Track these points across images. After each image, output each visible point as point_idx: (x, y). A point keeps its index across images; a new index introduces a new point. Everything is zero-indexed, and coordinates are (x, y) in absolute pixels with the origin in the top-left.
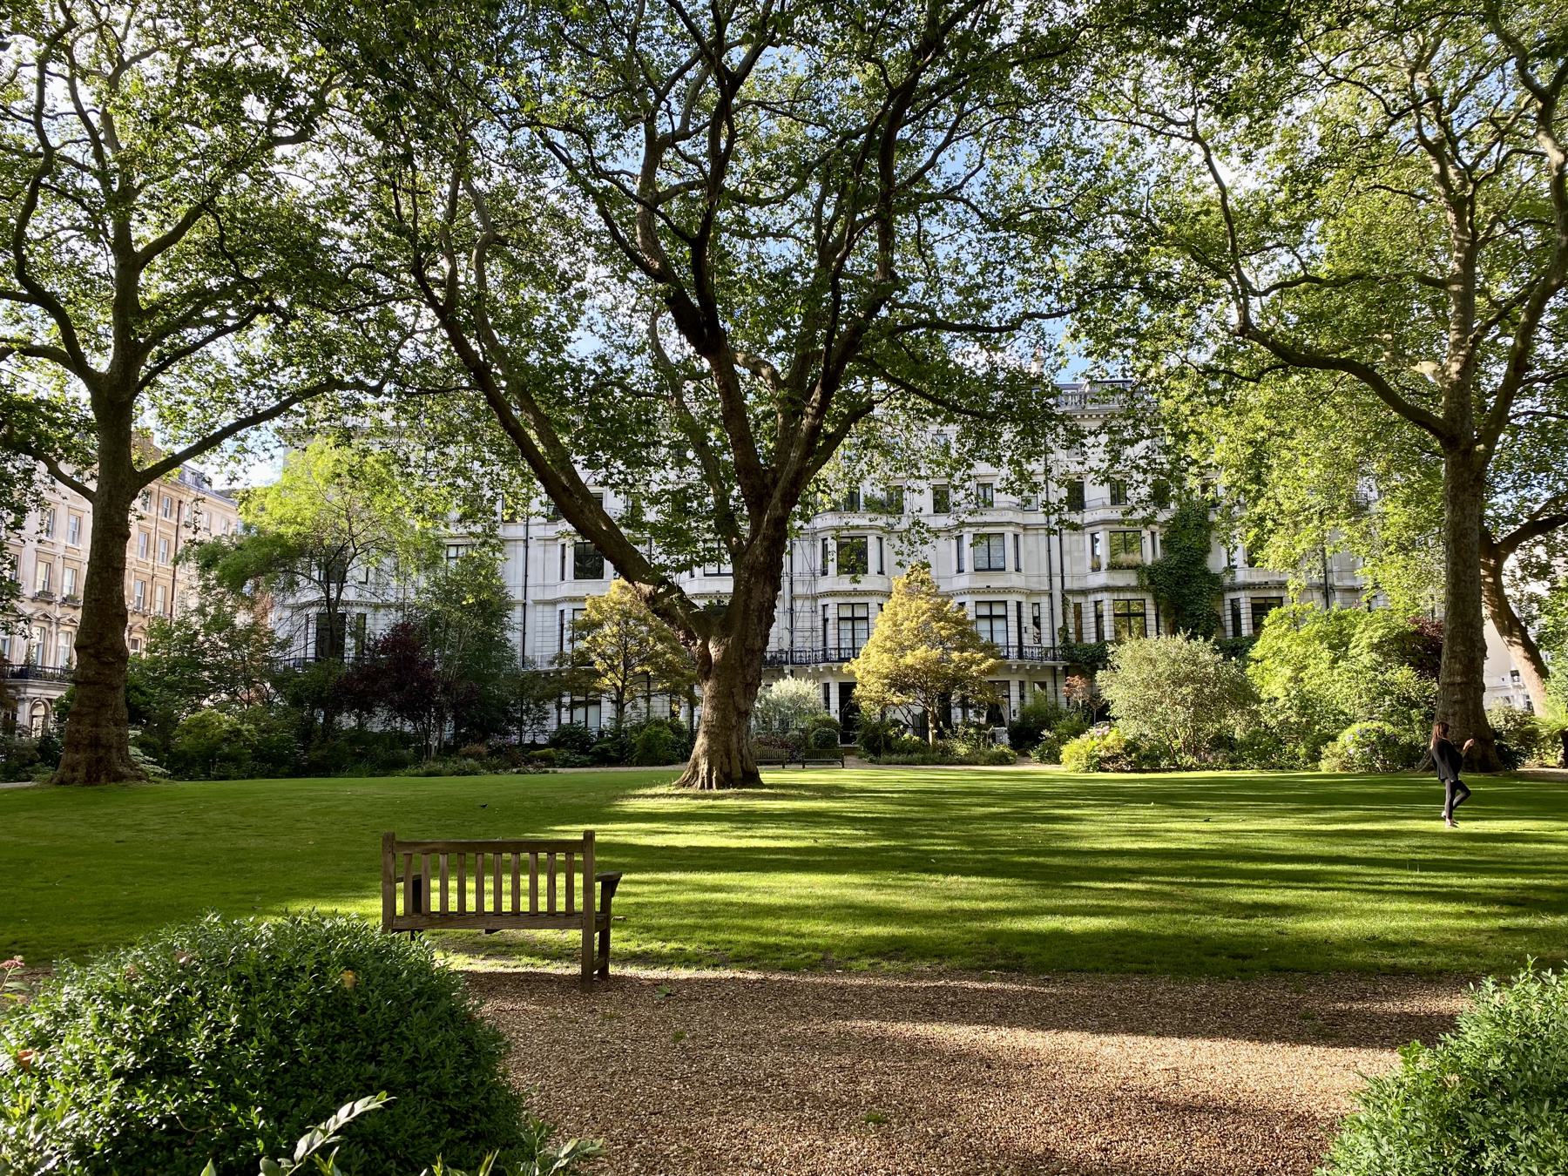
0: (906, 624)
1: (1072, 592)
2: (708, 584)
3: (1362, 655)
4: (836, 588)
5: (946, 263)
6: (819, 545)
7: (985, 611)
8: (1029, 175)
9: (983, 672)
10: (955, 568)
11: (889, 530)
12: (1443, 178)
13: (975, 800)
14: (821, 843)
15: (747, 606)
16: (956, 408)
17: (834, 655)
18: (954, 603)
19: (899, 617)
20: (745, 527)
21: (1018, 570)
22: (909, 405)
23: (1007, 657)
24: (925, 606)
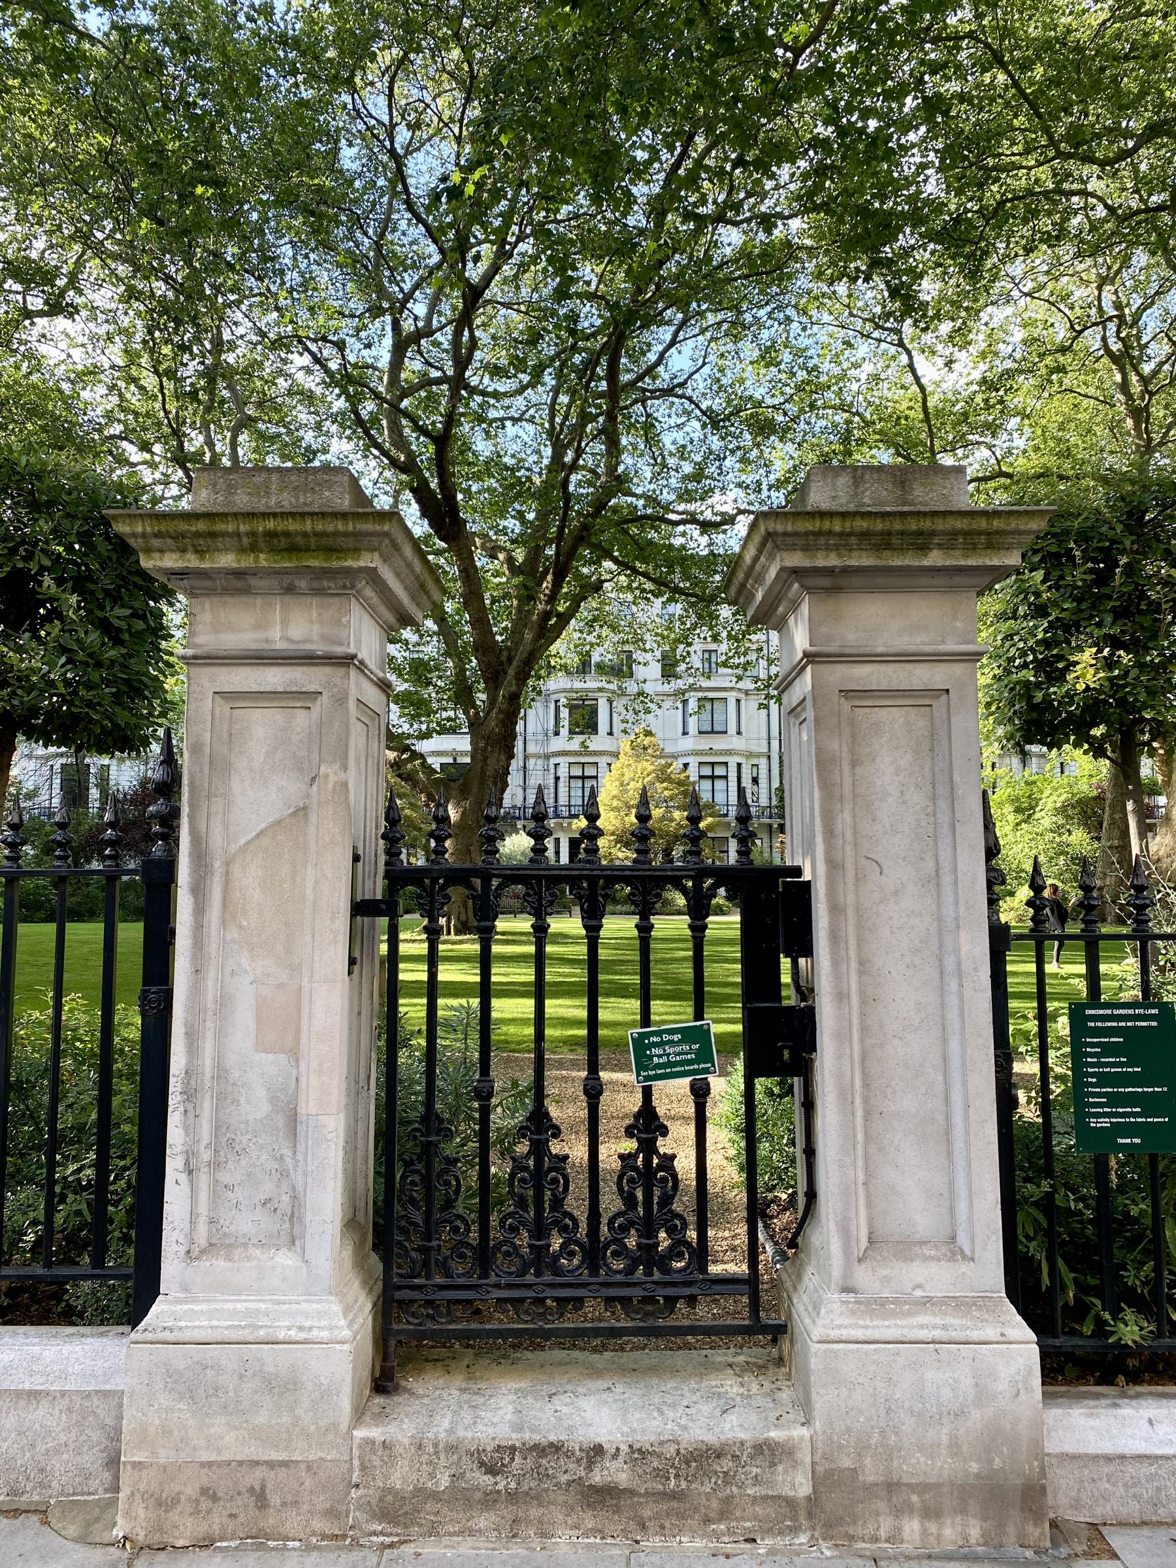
0: (632, 785)
2: (448, 748)
3: (1045, 819)
5: (673, 448)
6: (552, 706)
7: (707, 771)
8: (750, 368)
10: (680, 730)
12: (1124, 387)
13: (680, 945)
15: (483, 773)
16: (677, 590)
17: (564, 811)
18: (677, 765)
19: (626, 778)
20: (481, 697)
21: (739, 733)
23: (726, 815)
24: (651, 768)
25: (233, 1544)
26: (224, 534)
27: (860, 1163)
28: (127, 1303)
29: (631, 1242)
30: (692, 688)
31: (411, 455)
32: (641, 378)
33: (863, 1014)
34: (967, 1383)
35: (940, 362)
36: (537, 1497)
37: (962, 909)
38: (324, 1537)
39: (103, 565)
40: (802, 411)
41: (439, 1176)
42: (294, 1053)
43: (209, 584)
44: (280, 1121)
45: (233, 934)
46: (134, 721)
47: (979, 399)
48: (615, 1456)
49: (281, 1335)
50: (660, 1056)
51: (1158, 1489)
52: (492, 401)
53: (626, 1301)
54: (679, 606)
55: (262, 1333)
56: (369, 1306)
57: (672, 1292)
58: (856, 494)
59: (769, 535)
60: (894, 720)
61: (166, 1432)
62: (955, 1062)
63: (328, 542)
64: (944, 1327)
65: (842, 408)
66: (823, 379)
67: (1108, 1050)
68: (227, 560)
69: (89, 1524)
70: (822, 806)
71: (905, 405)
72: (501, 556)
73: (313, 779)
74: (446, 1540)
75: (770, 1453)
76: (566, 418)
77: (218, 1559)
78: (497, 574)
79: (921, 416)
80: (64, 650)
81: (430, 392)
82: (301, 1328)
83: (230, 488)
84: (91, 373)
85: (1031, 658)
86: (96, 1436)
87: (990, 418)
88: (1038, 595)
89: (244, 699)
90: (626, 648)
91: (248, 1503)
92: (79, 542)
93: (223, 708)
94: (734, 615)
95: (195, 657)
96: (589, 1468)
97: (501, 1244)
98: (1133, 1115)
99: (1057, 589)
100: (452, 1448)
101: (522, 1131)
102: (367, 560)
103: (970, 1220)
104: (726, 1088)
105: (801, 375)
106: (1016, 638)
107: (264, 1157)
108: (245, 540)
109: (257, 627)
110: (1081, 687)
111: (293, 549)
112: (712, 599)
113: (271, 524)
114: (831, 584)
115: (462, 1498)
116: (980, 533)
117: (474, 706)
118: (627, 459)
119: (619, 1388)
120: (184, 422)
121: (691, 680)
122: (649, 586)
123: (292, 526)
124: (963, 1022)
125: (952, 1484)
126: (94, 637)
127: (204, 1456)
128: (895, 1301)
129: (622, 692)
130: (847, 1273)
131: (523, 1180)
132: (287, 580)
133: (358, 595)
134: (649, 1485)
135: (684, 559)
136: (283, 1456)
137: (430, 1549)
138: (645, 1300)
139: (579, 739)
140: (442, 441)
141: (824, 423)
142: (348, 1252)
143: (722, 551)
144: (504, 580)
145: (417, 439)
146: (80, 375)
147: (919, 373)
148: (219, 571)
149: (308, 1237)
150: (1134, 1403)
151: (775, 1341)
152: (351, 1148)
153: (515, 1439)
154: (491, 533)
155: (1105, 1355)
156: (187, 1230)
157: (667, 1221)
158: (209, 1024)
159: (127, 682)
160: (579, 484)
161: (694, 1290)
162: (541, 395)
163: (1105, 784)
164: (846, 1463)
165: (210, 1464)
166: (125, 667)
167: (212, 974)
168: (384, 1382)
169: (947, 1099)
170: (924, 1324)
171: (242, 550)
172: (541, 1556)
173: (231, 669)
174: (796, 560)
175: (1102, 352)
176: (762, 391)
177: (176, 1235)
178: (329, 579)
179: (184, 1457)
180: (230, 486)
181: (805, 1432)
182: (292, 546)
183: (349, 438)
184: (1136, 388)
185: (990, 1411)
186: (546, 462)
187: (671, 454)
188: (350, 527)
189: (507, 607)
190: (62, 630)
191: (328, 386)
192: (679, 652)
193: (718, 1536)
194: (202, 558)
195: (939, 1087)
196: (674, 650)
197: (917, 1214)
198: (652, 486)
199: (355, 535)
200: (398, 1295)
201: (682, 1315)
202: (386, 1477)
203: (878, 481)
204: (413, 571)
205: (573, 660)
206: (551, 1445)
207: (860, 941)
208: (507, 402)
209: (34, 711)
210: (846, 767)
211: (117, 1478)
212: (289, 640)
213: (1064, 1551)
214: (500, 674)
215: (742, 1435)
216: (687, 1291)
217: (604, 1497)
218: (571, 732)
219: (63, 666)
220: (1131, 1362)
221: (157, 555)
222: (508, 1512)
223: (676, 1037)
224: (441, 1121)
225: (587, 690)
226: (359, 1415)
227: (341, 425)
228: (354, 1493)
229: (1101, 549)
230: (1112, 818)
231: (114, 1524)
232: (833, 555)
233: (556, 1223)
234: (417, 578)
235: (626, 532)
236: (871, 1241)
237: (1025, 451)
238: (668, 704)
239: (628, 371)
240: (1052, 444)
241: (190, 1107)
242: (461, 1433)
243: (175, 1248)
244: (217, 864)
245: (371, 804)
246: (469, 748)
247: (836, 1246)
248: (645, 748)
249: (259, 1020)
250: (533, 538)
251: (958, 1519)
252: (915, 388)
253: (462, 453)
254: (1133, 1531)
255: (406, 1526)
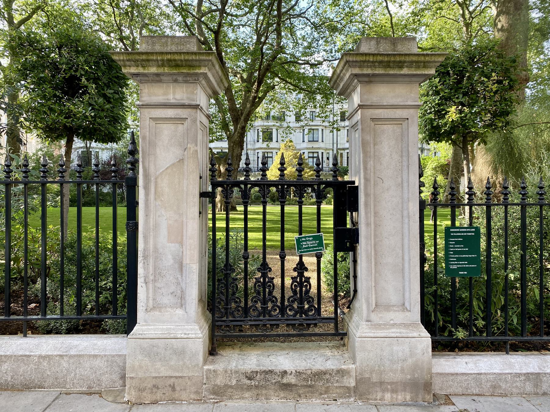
1: (340, 149)
4: (262, 147)
5: (300, 37)
6: (256, 131)
7: (311, 155)
8: (329, 7)
9: (309, 176)
11: (281, 127)
14: (255, 226)
20: (232, 128)
21: (323, 141)
22: (286, 87)
24: (291, 154)
25: (164, 402)
26: (152, 60)
27: (373, 280)
28: (125, 328)
29: (295, 306)
30: (306, 125)
31: (205, 38)
32: (289, 10)
33: (375, 231)
34: (407, 350)
35: (397, 5)
36: (265, 387)
37: (410, 195)
38: (194, 400)
39: (103, 74)
40: (347, 23)
41: (230, 284)
42: (181, 243)
43: (147, 78)
44: (177, 266)
45: (159, 203)
46: (116, 131)
47: (411, 19)
48: (291, 374)
49: (179, 336)
50: (305, 245)
51: (468, 384)
52: (235, 18)
53: (293, 325)
54: (302, 95)
55: (172, 335)
56: (207, 327)
57: (309, 322)
58: (378, 48)
59: (347, 62)
60: (388, 128)
61: (141, 367)
62: (406, 246)
63: (190, 63)
64: (400, 333)
65: (362, 22)
66: (355, 11)
67: (457, 243)
68: (153, 70)
69: (116, 397)
70: (363, 159)
71: (384, 22)
72: (238, 76)
73: (185, 149)
74: (235, 401)
75: (341, 373)
76: (262, 24)
77: (160, 407)
78: (237, 83)
79: (390, 26)
80: (90, 105)
81: (212, 15)
82: (185, 334)
83: (153, 44)
84: (87, 6)
85: (433, 110)
86: (117, 369)
87: (415, 27)
88: (436, 87)
89: (160, 120)
90: (283, 110)
91: (168, 389)
92: (94, 66)
93: (153, 123)
94: (322, 98)
95: (143, 105)
96: (282, 378)
97: (251, 306)
98: (464, 264)
99: (444, 85)
100: (236, 372)
101: (259, 269)
102: (203, 70)
103: (410, 298)
104: (328, 256)
105: (347, 10)
106: (428, 103)
107: (172, 278)
108: (160, 62)
109: (164, 94)
110: (450, 120)
111: (177, 66)
112: (314, 93)
113: (169, 57)
114: (368, 80)
115: (240, 387)
116: (421, 62)
117: (229, 131)
118: (284, 41)
119: (291, 353)
120: (122, 25)
121: (306, 122)
122: (292, 87)
123: (177, 57)
124: (409, 233)
125: (401, 382)
126: (101, 100)
127: (154, 375)
128: (384, 325)
129: (281, 127)
130: (368, 316)
131: (259, 286)
132: (175, 77)
133: (200, 83)
134: (302, 383)
135: (304, 77)
136: (180, 375)
137: (230, 403)
138: (299, 325)
139: (266, 143)
140: (217, 33)
141: (355, 28)
142: (200, 310)
143: (318, 75)
144: (239, 84)
145: (208, 32)
146: (83, 7)
147: (390, 10)
148: (151, 74)
149: (187, 304)
150: (461, 357)
151: (342, 339)
152: (200, 276)
153: (258, 369)
154: (235, 67)
155: (451, 342)
156: (145, 302)
157: (307, 299)
158: (151, 233)
159: (113, 117)
160: (267, 49)
161: (316, 322)
162: (253, 16)
163: (450, 160)
164: (367, 376)
165: (156, 377)
166: (112, 112)
167: (152, 216)
168: (212, 352)
169: (403, 259)
170: (394, 332)
171: (159, 66)
172: (266, 406)
173: (156, 109)
174: (357, 71)
175: (456, 2)
176: (333, 15)
177: (142, 304)
178: (190, 77)
179: (147, 375)
180: (153, 43)
181: (353, 366)
182: (177, 65)
183: (183, 32)
184: (467, 16)
185: (414, 359)
186: (254, 41)
187: (300, 39)
188: (198, 58)
189: (241, 95)
190: (89, 98)
191: (174, 11)
192: (302, 112)
193: (324, 399)
194: (144, 69)
195: (400, 255)
196: (300, 111)
197: (391, 295)
198: (293, 51)
199: (200, 61)
200: (217, 323)
201: (311, 331)
202: (215, 381)
203: (386, 43)
204: (219, 75)
205: (264, 114)
206: (270, 371)
207: (375, 206)
208: (240, 18)
209: (80, 127)
210: (372, 146)
211: (124, 382)
212: (175, 99)
213: (437, 403)
214: (237, 119)
215: (333, 367)
216: (314, 322)
217: (287, 387)
218: (263, 141)
219: (91, 110)
220: (460, 345)
221: (128, 68)
222: (255, 392)
223: (311, 239)
224: (231, 266)
225: (269, 126)
226: (205, 362)
227: (180, 27)
228: (204, 386)
229: (459, 71)
230: (452, 171)
231: (124, 397)
232: (369, 69)
233: (270, 300)
234: (220, 77)
235: (283, 67)
236: (376, 305)
237: (426, 39)
238: (298, 131)
239: (285, 7)
240: (436, 36)
241: (145, 261)
242: (240, 367)
243: (142, 308)
244: (152, 179)
245: (205, 159)
246: (227, 146)
247: (364, 307)
248: (290, 147)
249: (169, 233)
250: (250, 69)
251: (403, 393)
252: (388, 15)
253: (224, 37)
254: (460, 397)
255: (221, 396)
